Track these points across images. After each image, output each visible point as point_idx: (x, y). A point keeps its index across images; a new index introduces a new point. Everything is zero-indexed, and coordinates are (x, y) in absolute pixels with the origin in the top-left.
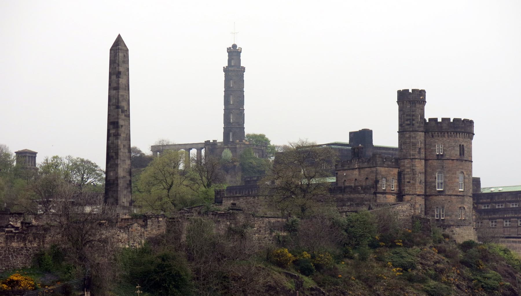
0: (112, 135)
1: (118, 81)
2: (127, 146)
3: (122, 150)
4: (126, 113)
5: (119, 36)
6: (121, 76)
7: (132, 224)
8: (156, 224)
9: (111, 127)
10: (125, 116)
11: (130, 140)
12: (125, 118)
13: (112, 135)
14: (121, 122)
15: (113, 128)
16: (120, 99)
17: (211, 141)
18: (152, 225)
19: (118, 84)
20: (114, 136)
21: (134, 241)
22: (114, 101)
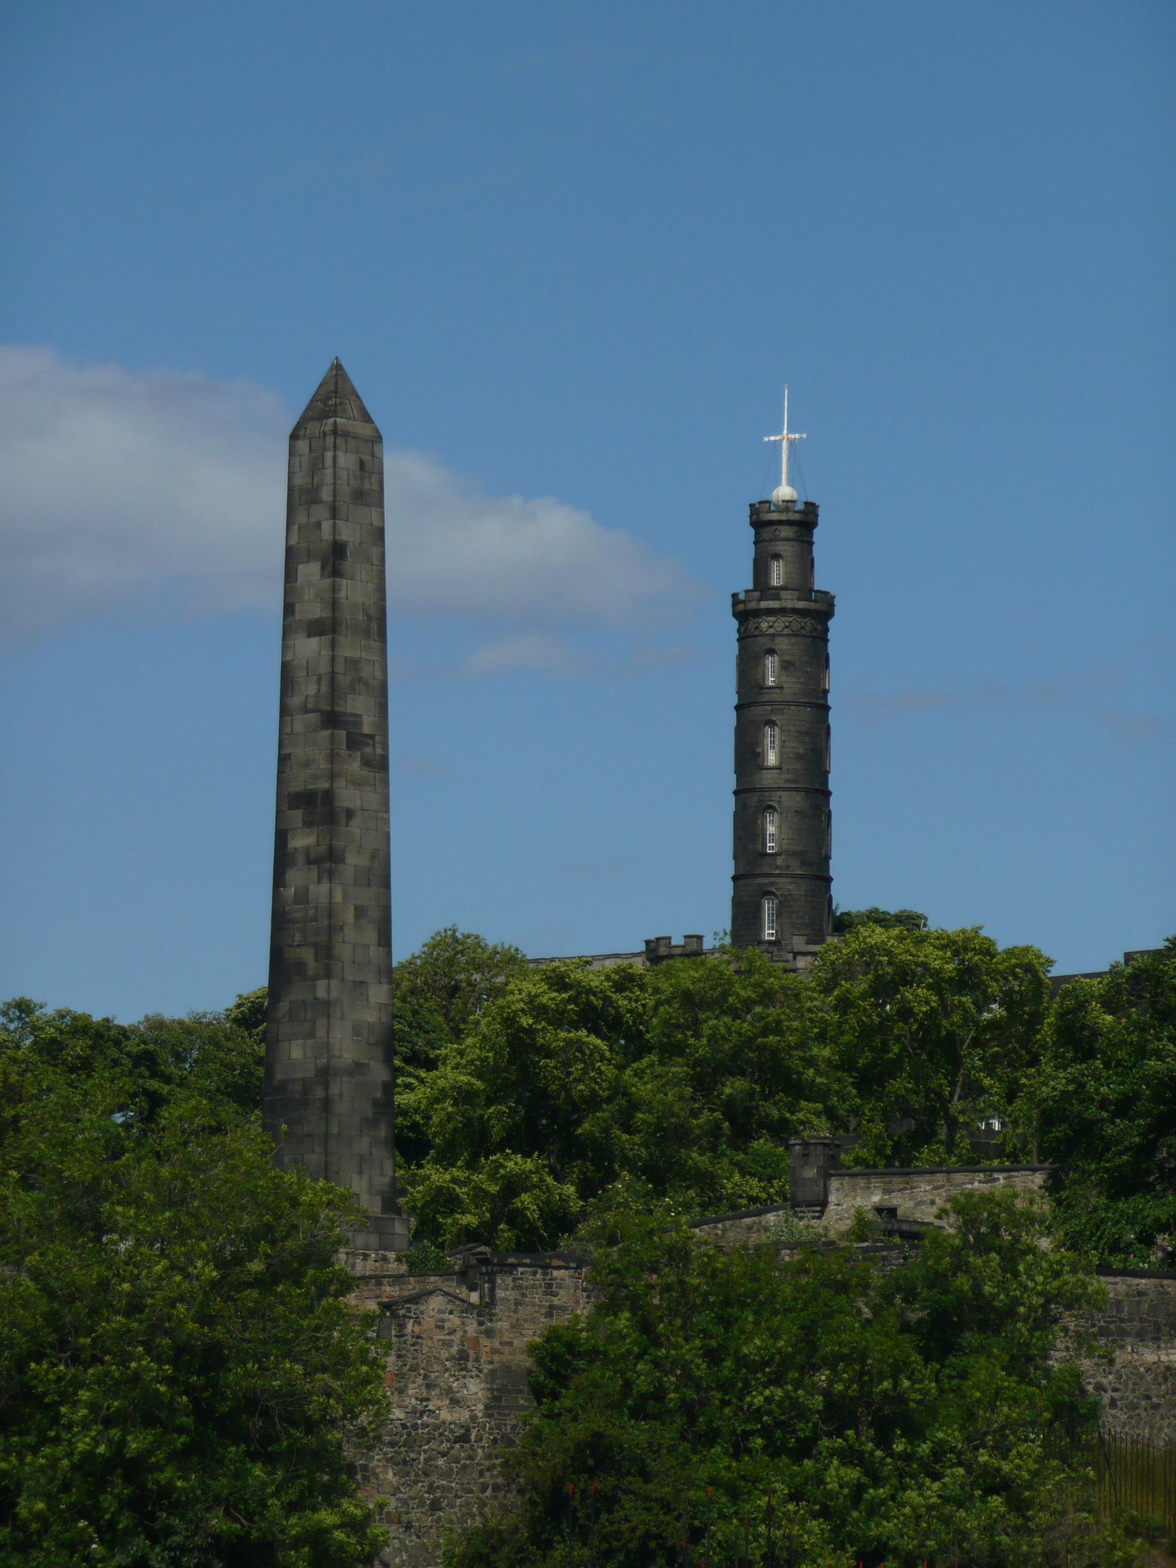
0: (300, 859)
1: (334, 589)
2: (374, 914)
3: (348, 931)
4: (368, 750)
5: (337, 369)
6: (348, 565)
7: (414, 1299)
8: (538, 1297)
9: (297, 816)
10: (366, 763)
11: (387, 884)
12: (366, 772)
13: (300, 859)
14: (347, 796)
15: (308, 824)
16: (343, 681)
17: (678, 940)
18: (518, 1303)
19: (334, 605)
20: (309, 861)
21: (429, 1386)
22: (311, 689)
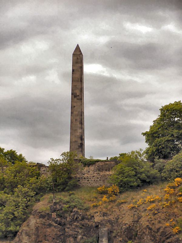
5: (78, 45)
